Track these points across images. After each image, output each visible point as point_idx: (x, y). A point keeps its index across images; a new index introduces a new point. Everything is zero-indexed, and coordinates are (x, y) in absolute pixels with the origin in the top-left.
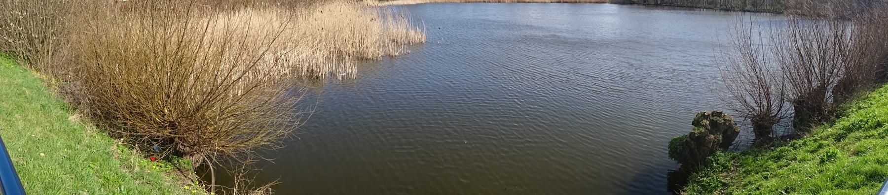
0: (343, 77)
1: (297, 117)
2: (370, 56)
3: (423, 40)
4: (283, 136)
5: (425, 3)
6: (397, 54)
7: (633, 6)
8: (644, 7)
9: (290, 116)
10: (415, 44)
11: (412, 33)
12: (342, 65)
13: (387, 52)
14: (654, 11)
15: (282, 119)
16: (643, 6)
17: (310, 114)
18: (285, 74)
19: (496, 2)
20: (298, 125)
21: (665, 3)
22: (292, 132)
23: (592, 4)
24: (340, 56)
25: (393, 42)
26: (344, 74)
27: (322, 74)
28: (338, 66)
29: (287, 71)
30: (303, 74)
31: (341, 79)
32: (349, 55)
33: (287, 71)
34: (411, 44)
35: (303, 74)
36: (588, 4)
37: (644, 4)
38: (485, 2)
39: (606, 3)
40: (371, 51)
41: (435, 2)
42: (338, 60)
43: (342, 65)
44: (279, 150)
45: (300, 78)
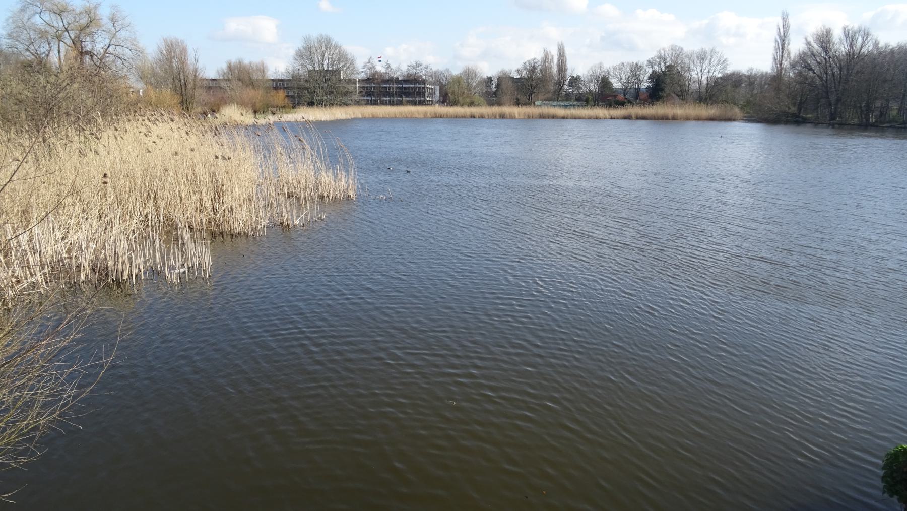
0: (181, 277)
1: (71, 378)
2: (239, 228)
3: (351, 193)
4: (36, 429)
5: (352, 119)
6: (297, 222)
7: (801, 129)
8: (829, 131)
9: (51, 380)
10: (335, 201)
11: (326, 178)
12: (177, 251)
13: (276, 218)
14: (872, 141)
15: (30, 390)
16: (828, 127)
17: (102, 366)
18: (34, 285)
19: (495, 118)
20: (74, 398)
21: (889, 122)
22: (59, 416)
23: (700, 122)
24: (171, 233)
25: (289, 196)
26: (182, 270)
27: (130, 275)
28: (168, 253)
29: (39, 277)
30: (83, 277)
31: (175, 280)
32: (191, 229)
33: (39, 277)
34: (327, 201)
35: (83, 277)
36: (693, 123)
37: (830, 124)
38: (474, 117)
39: (734, 120)
40: (240, 220)
41: (373, 117)
42: (167, 242)
43: (177, 251)
44: (25, 465)
45: (74, 287)
